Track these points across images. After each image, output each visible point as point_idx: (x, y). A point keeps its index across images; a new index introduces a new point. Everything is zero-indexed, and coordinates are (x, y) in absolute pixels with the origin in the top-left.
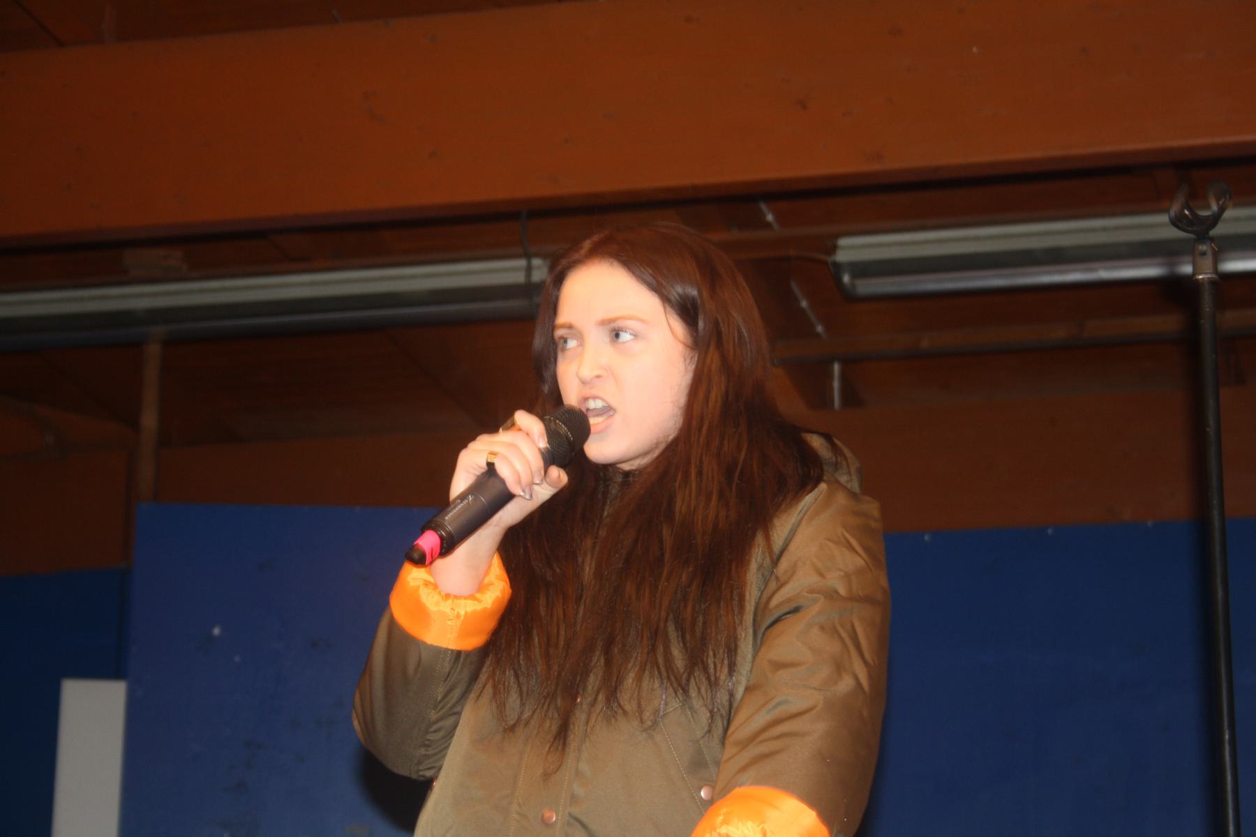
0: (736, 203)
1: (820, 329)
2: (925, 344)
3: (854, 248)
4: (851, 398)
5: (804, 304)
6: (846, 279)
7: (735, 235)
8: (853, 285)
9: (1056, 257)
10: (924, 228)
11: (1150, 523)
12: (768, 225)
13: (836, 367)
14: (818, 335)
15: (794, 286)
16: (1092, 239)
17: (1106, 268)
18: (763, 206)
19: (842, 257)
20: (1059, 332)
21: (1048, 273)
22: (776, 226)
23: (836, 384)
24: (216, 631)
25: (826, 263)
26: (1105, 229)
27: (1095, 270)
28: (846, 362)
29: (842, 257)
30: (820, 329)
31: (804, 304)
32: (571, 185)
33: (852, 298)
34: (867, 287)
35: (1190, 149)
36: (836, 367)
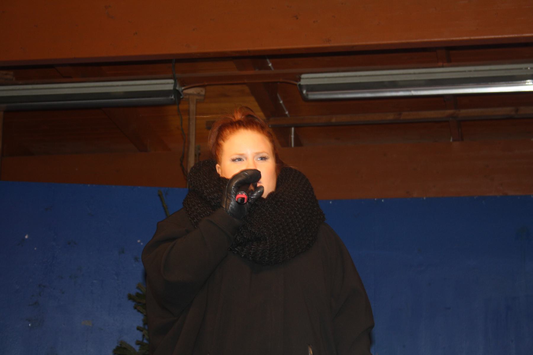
0: (258, 58)
1: (287, 113)
2: (334, 120)
3: (308, 79)
4: (298, 143)
5: (281, 102)
6: (304, 92)
7: (257, 72)
8: (307, 95)
9: (394, 85)
10: (338, 71)
11: (425, 198)
12: (269, 68)
13: (293, 129)
14: (286, 115)
15: (278, 95)
16: (409, 78)
17: (325, 94)
18: (268, 60)
19: (302, 82)
20: (390, 117)
21: (340, 94)
23: (293, 136)
24: (26, 237)
25: (296, 85)
26: (414, 74)
27: (410, 91)
28: (296, 127)
29: (302, 82)
30: (287, 113)
31: (281, 102)
32: (194, 49)
33: (306, 100)
34: (314, 96)
35: (380, 45)
36: (293, 129)
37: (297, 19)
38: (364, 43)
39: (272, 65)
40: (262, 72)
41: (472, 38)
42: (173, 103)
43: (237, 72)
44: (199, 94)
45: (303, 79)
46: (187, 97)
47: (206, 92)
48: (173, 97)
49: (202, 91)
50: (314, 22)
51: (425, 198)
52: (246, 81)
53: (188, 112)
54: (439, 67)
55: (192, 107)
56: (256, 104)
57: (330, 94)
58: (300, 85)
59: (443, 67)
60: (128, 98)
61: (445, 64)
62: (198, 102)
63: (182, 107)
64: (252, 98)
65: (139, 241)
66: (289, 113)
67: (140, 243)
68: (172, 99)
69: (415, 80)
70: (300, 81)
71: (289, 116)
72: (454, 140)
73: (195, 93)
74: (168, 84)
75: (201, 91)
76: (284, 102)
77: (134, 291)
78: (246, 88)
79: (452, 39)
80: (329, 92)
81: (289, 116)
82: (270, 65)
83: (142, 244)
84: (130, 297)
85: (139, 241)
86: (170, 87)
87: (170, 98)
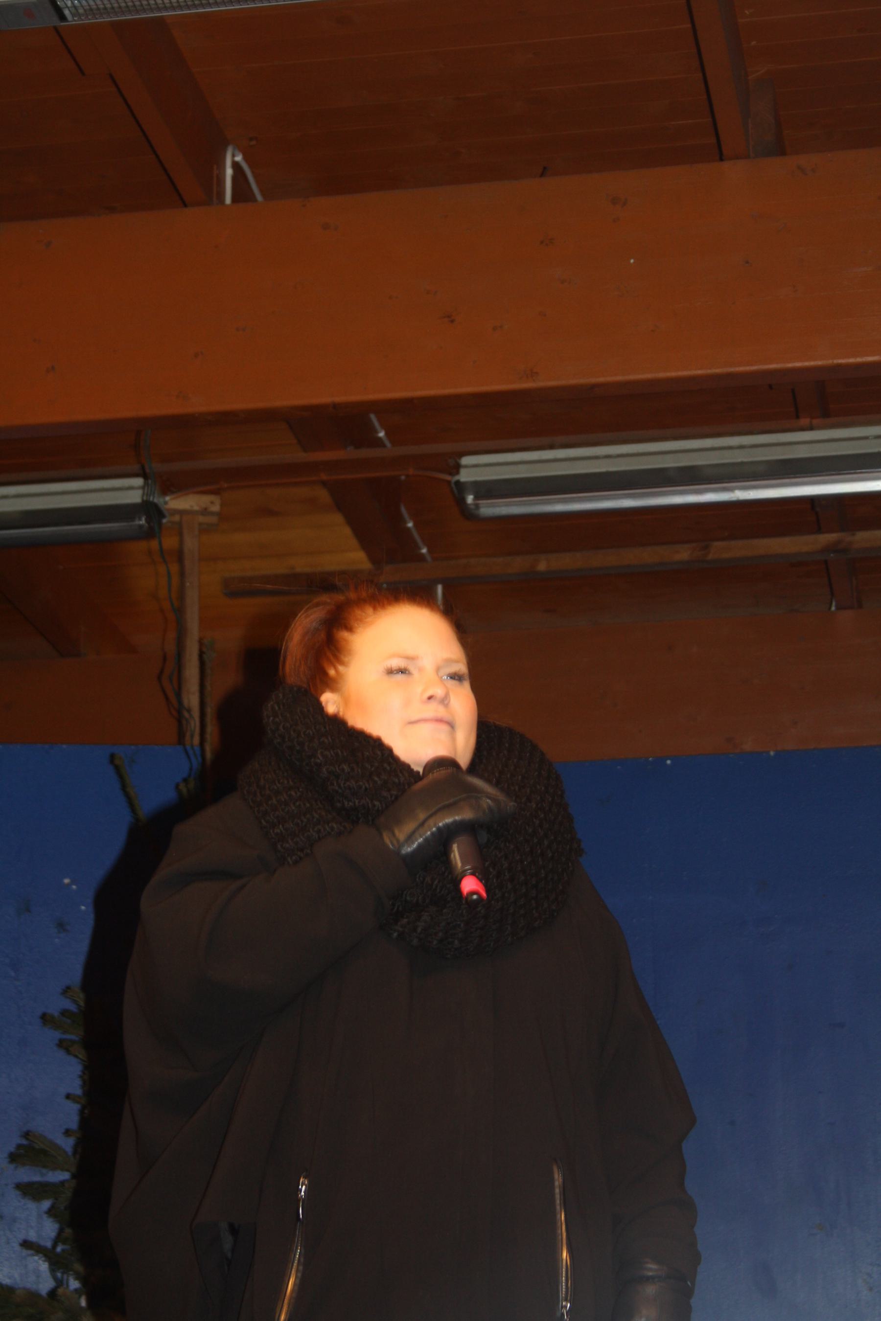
0: (345, 424)
1: (424, 551)
2: (542, 567)
3: (477, 467)
5: (410, 525)
6: (470, 499)
7: (349, 453)
8: (477, 506)
10: (552, 447)
11: (772, 753)
12: (379, 443)
14: (422, 558)
15: (403, 510)
19: (465, 476)
20: (683, 554)
22: (388, 444)
25: (449, 482)
27: (731, 490)
29: (465, 476)
30: (424, 551)
31: (410, 525)
37: (452, 321)
38: (619, 378)
39: (387, 434)
40: (365, 453)
41: (662, 375)
42: (150, 534)
43: (300, 456)
44: (205, 512)
45: (466, 467)
46: (177, 518)
47: (222, 505)
48: (143, 522)
49: (212, 503)
50: (495, 328)
51: (772, 753)
52: (324, 477)
53: (180, 556)
54: (803, 429)
55: (191, 544)
56: (347, 531)
57: (590, 500)
58: (458, 483)
59: (811, 428)
60: (56, 525)
61: (815, 422)
62: (205, 530)
63: (170, 542)
64: (338, 518)
65: (67, 881)
66: (429, 551)
67: (68, 885)
68: (141, 526)
69: (742, 463)
70: (458, 473)
71: (429, 558)
72: (838, 608)
73: (196, 508)
74: (131, 488)
75: (213, 503)
76: (415, 525)
77: (57, 1004)
78: (323, 495)
79: (836, 361)
80: (871, 475)
81: (429, 558)
82: (382, 434)
83: (74, 887)
84: (45, 1019)
85: (67, 881)
86: (135, 497)
87: (137, 522)
